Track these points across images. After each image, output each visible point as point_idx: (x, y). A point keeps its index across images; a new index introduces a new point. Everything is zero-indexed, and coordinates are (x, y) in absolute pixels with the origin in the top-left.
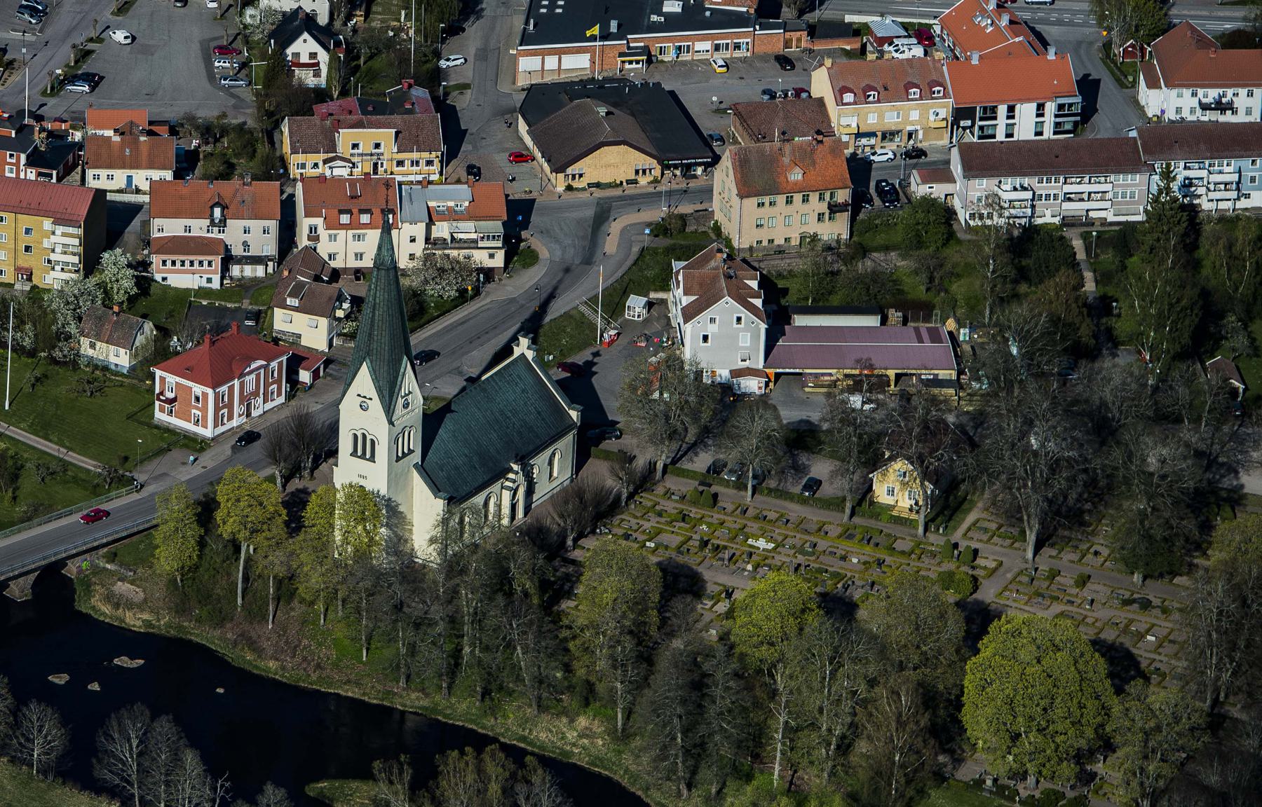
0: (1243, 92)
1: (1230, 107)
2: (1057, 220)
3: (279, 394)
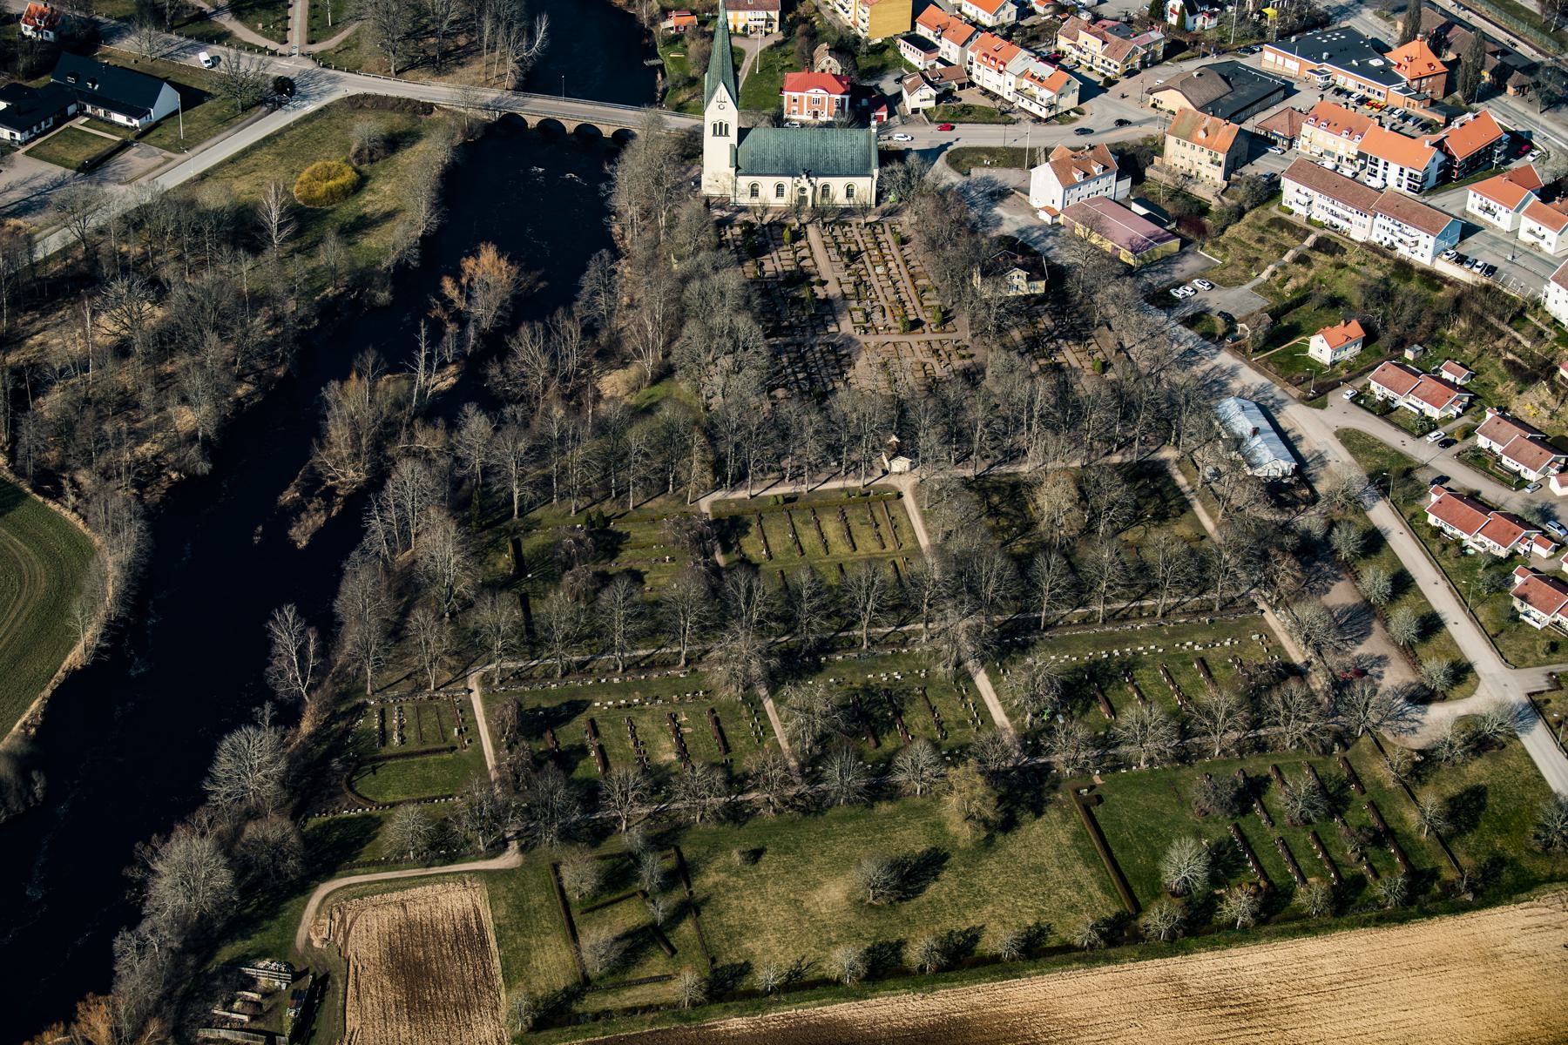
0: (1504, 209)
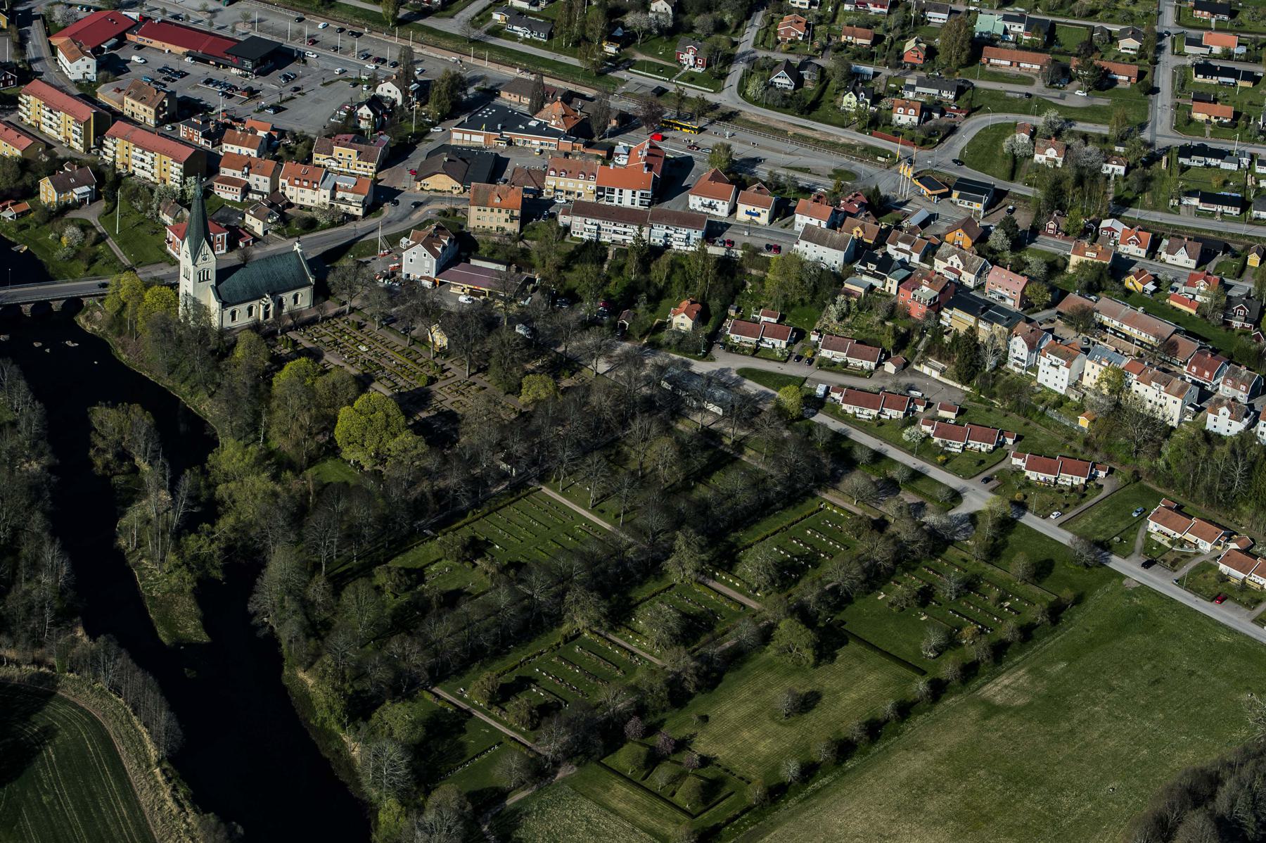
0: (721, 202)
1: (714, 208)
2: (610, 241)
3: (223, 249)
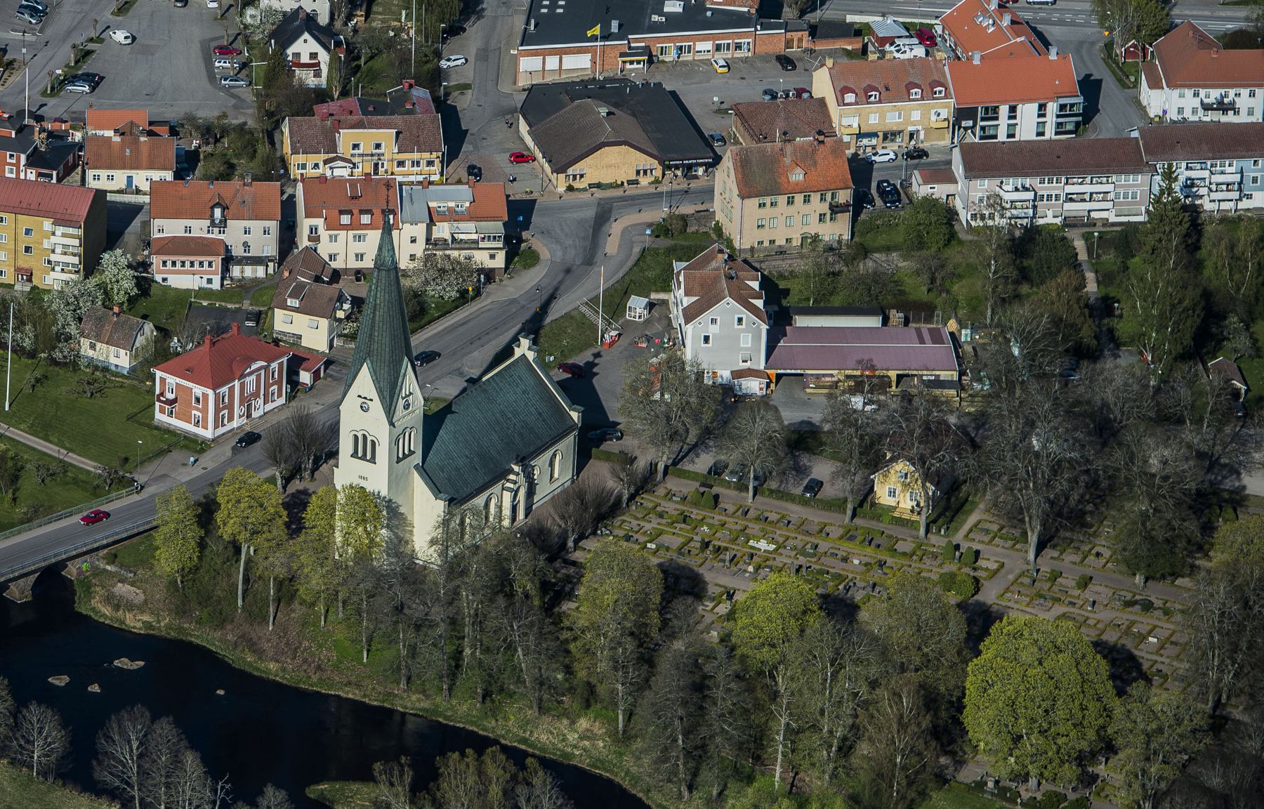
0: (1245, 92)
2: (1058, 221)
3: (280, 395)
